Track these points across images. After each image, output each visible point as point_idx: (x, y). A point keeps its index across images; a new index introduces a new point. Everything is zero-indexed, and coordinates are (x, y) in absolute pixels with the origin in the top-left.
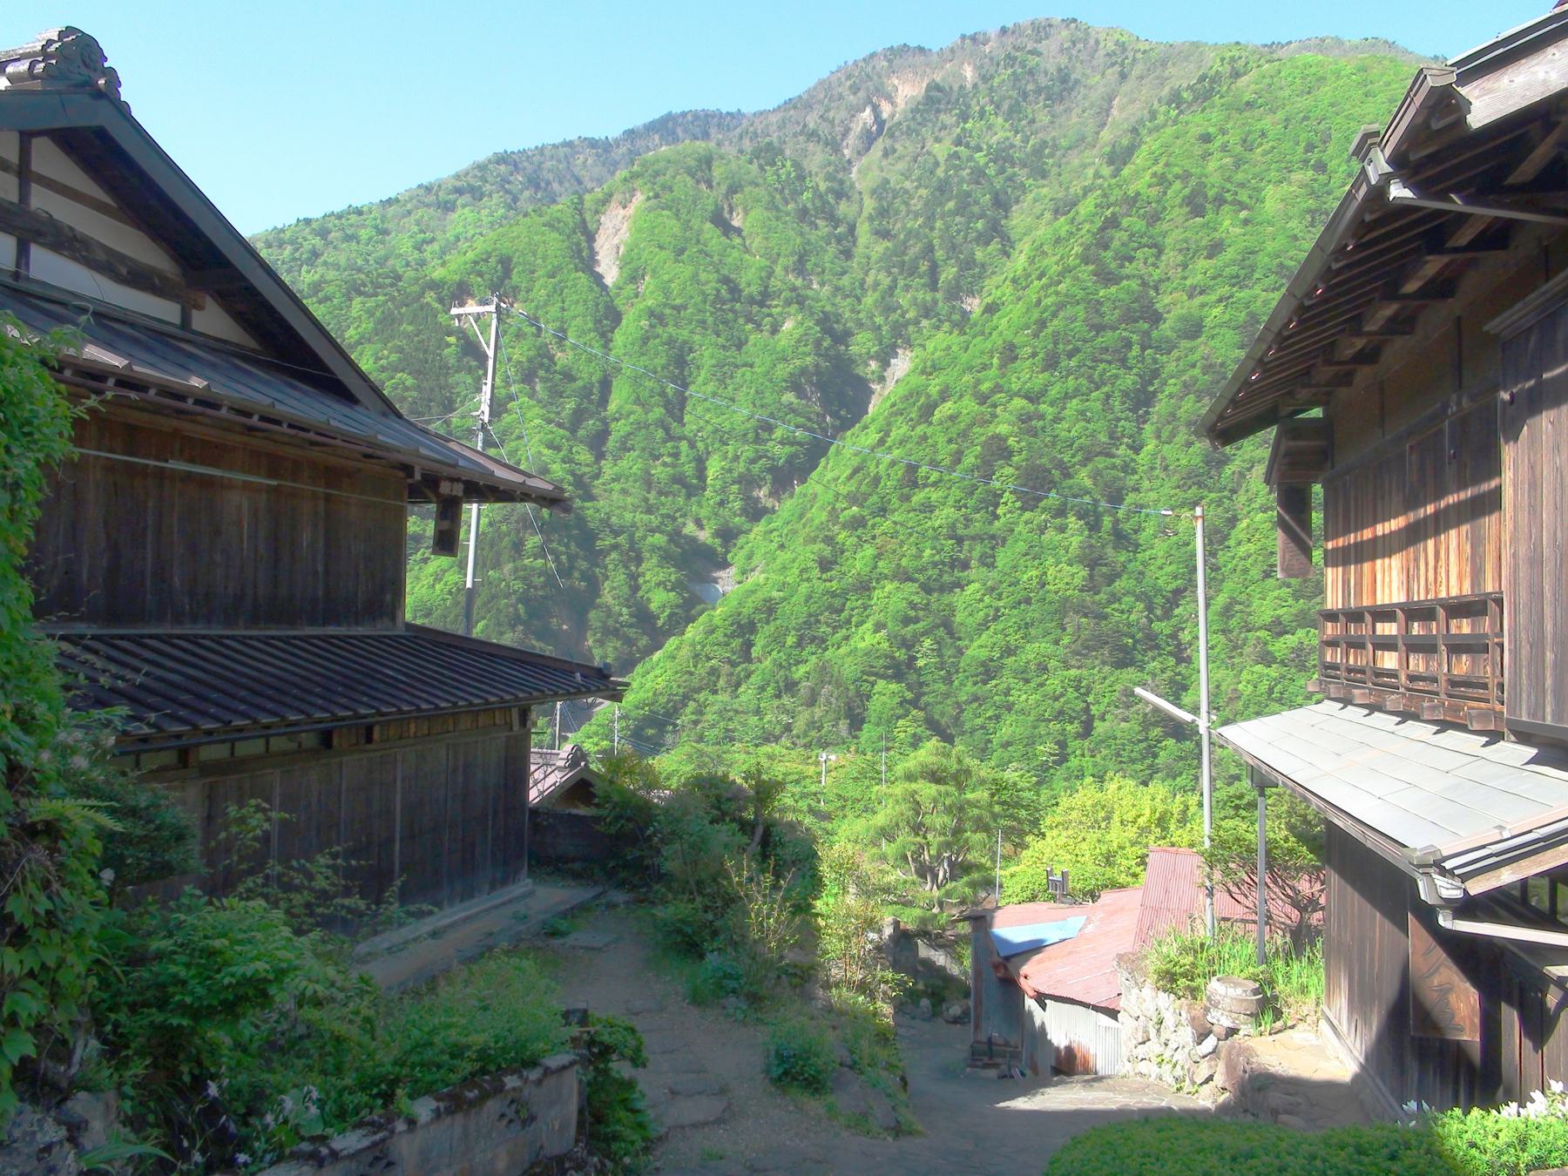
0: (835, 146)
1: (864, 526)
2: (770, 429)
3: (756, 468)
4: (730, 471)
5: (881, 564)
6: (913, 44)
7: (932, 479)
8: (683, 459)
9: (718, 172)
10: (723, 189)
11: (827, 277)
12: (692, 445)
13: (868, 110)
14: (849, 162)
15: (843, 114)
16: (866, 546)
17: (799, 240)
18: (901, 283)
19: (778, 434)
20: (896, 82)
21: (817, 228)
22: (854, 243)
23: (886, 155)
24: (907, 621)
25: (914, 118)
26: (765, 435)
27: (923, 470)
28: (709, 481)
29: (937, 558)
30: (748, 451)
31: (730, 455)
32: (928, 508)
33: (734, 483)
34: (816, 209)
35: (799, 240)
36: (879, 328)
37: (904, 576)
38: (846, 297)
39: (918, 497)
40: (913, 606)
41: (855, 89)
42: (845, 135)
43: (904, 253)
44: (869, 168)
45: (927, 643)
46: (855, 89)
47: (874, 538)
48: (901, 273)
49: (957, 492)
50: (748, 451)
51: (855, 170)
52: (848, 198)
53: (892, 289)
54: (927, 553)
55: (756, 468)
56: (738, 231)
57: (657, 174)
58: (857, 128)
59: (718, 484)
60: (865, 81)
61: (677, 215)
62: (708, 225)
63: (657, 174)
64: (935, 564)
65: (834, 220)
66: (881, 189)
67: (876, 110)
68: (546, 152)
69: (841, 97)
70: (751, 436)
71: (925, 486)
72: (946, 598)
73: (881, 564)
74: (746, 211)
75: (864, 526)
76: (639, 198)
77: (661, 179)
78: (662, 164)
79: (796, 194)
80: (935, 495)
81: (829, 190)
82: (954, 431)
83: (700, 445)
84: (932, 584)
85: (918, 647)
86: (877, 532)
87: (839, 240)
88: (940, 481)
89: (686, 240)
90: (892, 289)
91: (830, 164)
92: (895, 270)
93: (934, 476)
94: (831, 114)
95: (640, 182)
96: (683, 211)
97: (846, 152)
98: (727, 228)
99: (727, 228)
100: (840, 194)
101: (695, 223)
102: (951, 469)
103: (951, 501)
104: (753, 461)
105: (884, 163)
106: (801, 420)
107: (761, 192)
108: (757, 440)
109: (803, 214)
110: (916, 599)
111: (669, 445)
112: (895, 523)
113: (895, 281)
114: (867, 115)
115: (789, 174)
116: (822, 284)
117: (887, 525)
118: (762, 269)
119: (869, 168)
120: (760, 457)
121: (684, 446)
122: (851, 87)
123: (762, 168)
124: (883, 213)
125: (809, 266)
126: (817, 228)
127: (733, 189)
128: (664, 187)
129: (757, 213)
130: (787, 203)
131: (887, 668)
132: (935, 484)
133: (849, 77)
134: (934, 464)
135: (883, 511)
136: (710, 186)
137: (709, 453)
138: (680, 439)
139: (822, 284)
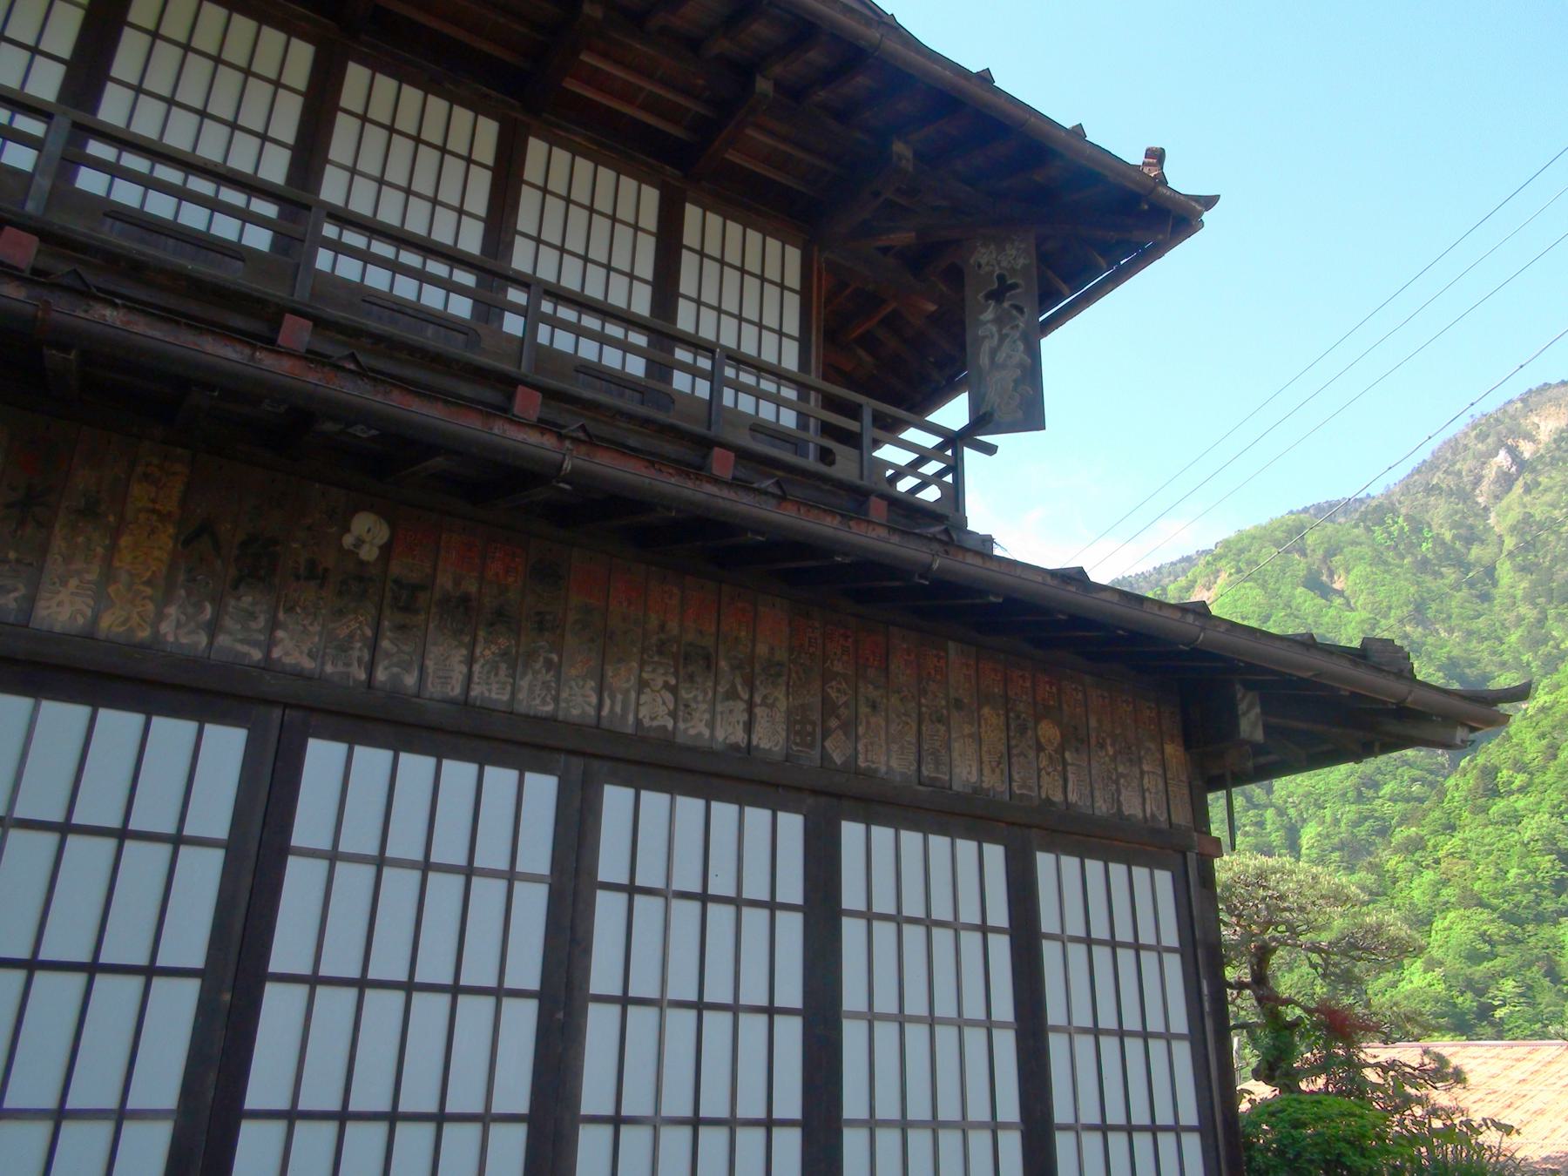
0: (1465, 496)
1: (1424, 848)
2: (1376, 786)
3: (1362, 832)
4: (1328, 836)
5: (1444, 892)
6: (1554, 381)
7: (1517, 783)
8: (1269, 827)
9: (1311, 539)
10: (1320, 553)
11: (1454, 622)
12: (1281, 812)
13: (1502, 453)
14: (1486, 509)
15: (1471, 463)
16: (1426, 872)
17: (1412, 590)
18: (1552, 613)
19: (1386, 790)
20: (1536, 420)
21: (1442, 576)
22: (1495, 584)
23: (1527, 490)
24: (1474, 957)
25: (1559, 448)
26: (1371, 793)
27: (1504, 774)
28: (1304, 851)
29: (1528, 878)
30: (1350, 812)
31: (1328, 819)
32: (1513, 819)
33: (1334, 850)
34: (1439, 557)
35: (1412, 590)
36: (1528, 664)
37: (1473, 901)
38: (1482, 640)
39: (1499, 807)
40: (1483, 936)
41: (1482, 437)
42: (1478, 480)
43: (1551, 580)
44: (1509, 508)
45: (1509, 985)
46: (1482, 437)
47: (1437, 862)
48: (1550, 602)
49: (1554, 796)
50: (1350, 812)
51: (1492, 515)
52: (1482, 542)
53: (1541, 621)
54: (1513, 872)
55: (1362, 832)
56: (1341, 593)
57: (1241, 551)
58: (1490, 473)
59: (1314, 853)
60: (1500, 429)
61: (1264, 586)
62: (1300, 590)
63: (1241, 551)
64: (1527, 888)
65: (1462, 564)
66: (1524, 525)
67: (1513, 452)
68: (1165, 571)
69: (1466, 447)
70: (1351, 795)
71: (1511, 793)
72: (1547, 931)
73: (1444, 892)
74: (1348, 571)
75: (1424, 848)
76: (1222, 580)
77: (1246, 555)
78: (1246, 541)
79: (1412, 547)
80: (1521, 803)
81: (1455, 537)
82: (1546, 724)
83: (1292, 812)
84: (1523, 913)
85: (1493, 992)
86: (1440, 854)
87: (1471, 584)
88: (1530, 784)
89: (1272, 606)
90: (1541, 621)
91: (1456, 512)
92: (1539, 600)
93: (1520, 779)
94: (1458, 466)
95: (1223, 562)
96: (1271, 582)
97: (1480, 500)
98: (1325, 591)
99: (1325, 591)
100: (1469, 540)
101: (1285, 590)
102: (1544, 769)
103: (1546, 806)
104: (1357, 823)
105: (1527, 499)
106: (1416, 773)
107: (1365, 550)
108: (1360, 798)
109: (1423, 565)
110: (1492, 929)
111: (1251, 813)
112: (1465, 840)
113: (1544, 612)
114: (1503, 459)
115: (1402, 528)
116: (1451, 631)
117: (1455, 842)
118: (1363, 621)
119: (1509, 508)
120: (1366, 818)
121: (1270, 814)
122: (1477, 437)
123: (1368, 529)
124: (1527, 546)
125: (1430, 614)
126: (1442, 576)
127: (1331, 553)
128: (1249, 563)
129: (1359, 570)
130: (1403, 558)
131: (1436, 1015)
132: (1522, 790)
133: (1474, 428)
134: (1520, 767)
135: (1451, 828)
136: (1303, 553)
137: (1304, 821)
138: (1266, 807)
139: (1451, 631)
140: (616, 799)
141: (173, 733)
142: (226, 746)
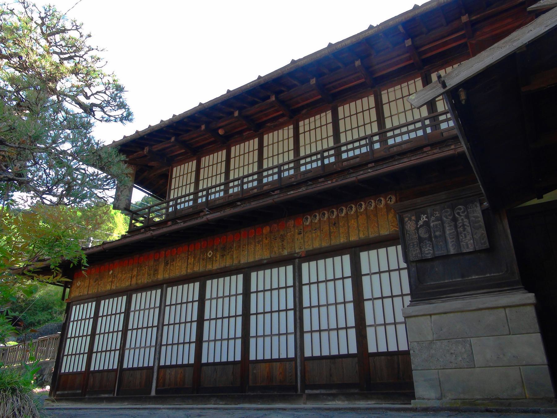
140: (364, 256)
141: (338, 259)
142: (347, 258)
